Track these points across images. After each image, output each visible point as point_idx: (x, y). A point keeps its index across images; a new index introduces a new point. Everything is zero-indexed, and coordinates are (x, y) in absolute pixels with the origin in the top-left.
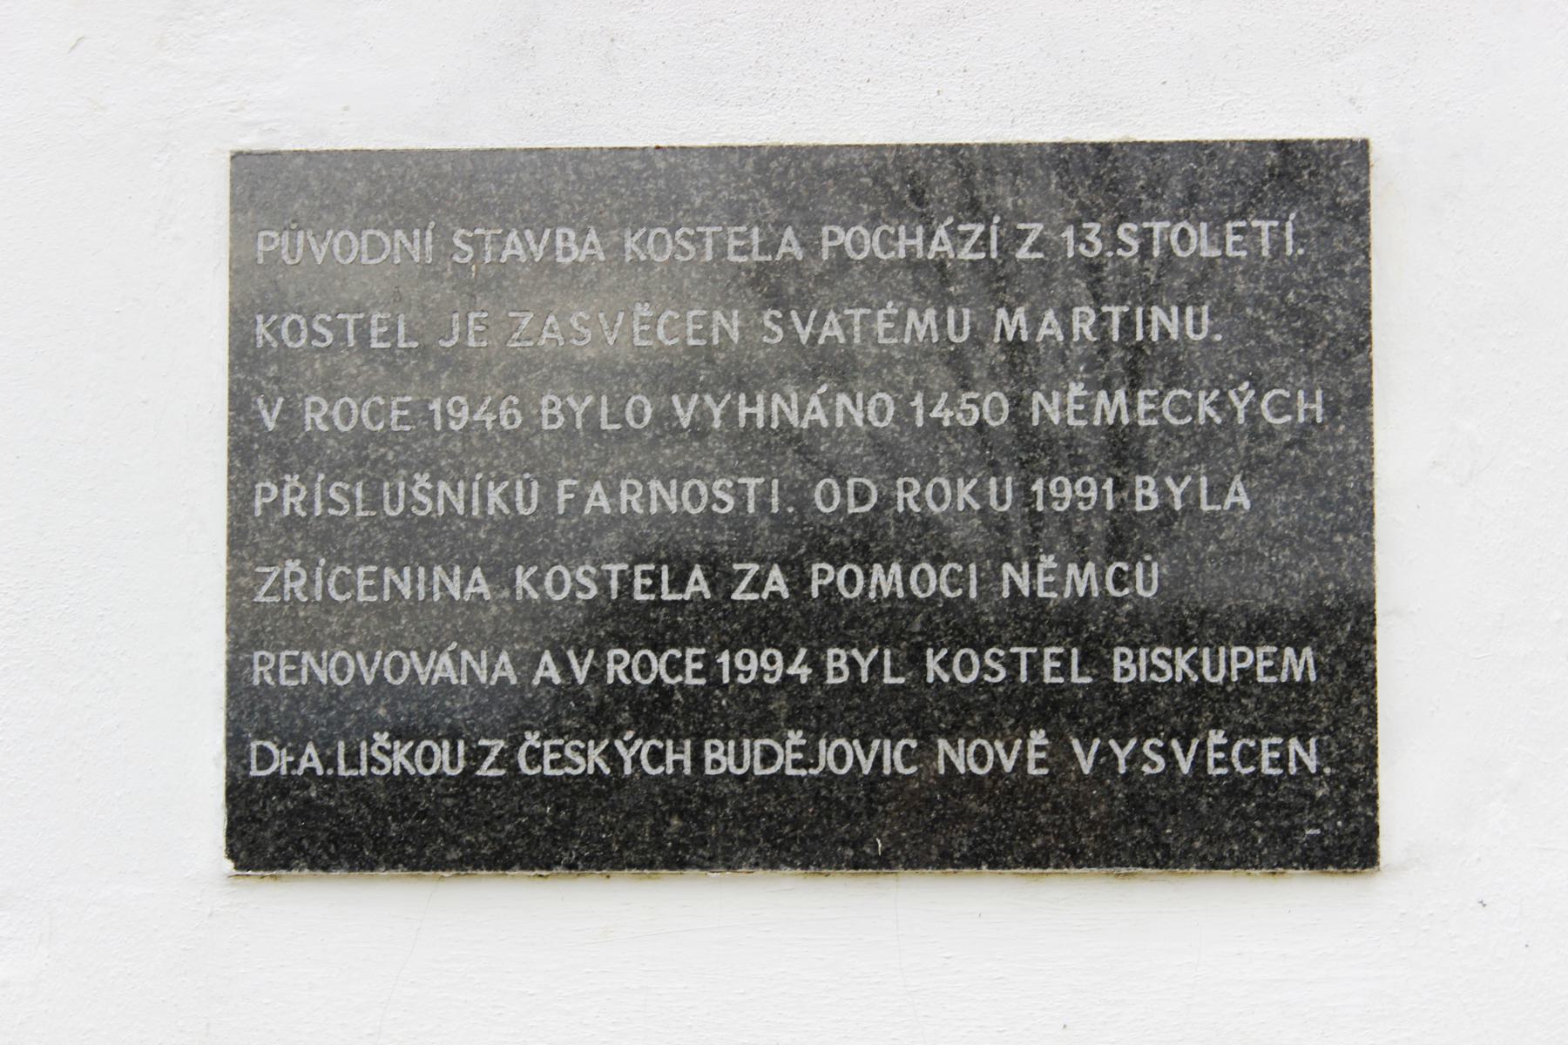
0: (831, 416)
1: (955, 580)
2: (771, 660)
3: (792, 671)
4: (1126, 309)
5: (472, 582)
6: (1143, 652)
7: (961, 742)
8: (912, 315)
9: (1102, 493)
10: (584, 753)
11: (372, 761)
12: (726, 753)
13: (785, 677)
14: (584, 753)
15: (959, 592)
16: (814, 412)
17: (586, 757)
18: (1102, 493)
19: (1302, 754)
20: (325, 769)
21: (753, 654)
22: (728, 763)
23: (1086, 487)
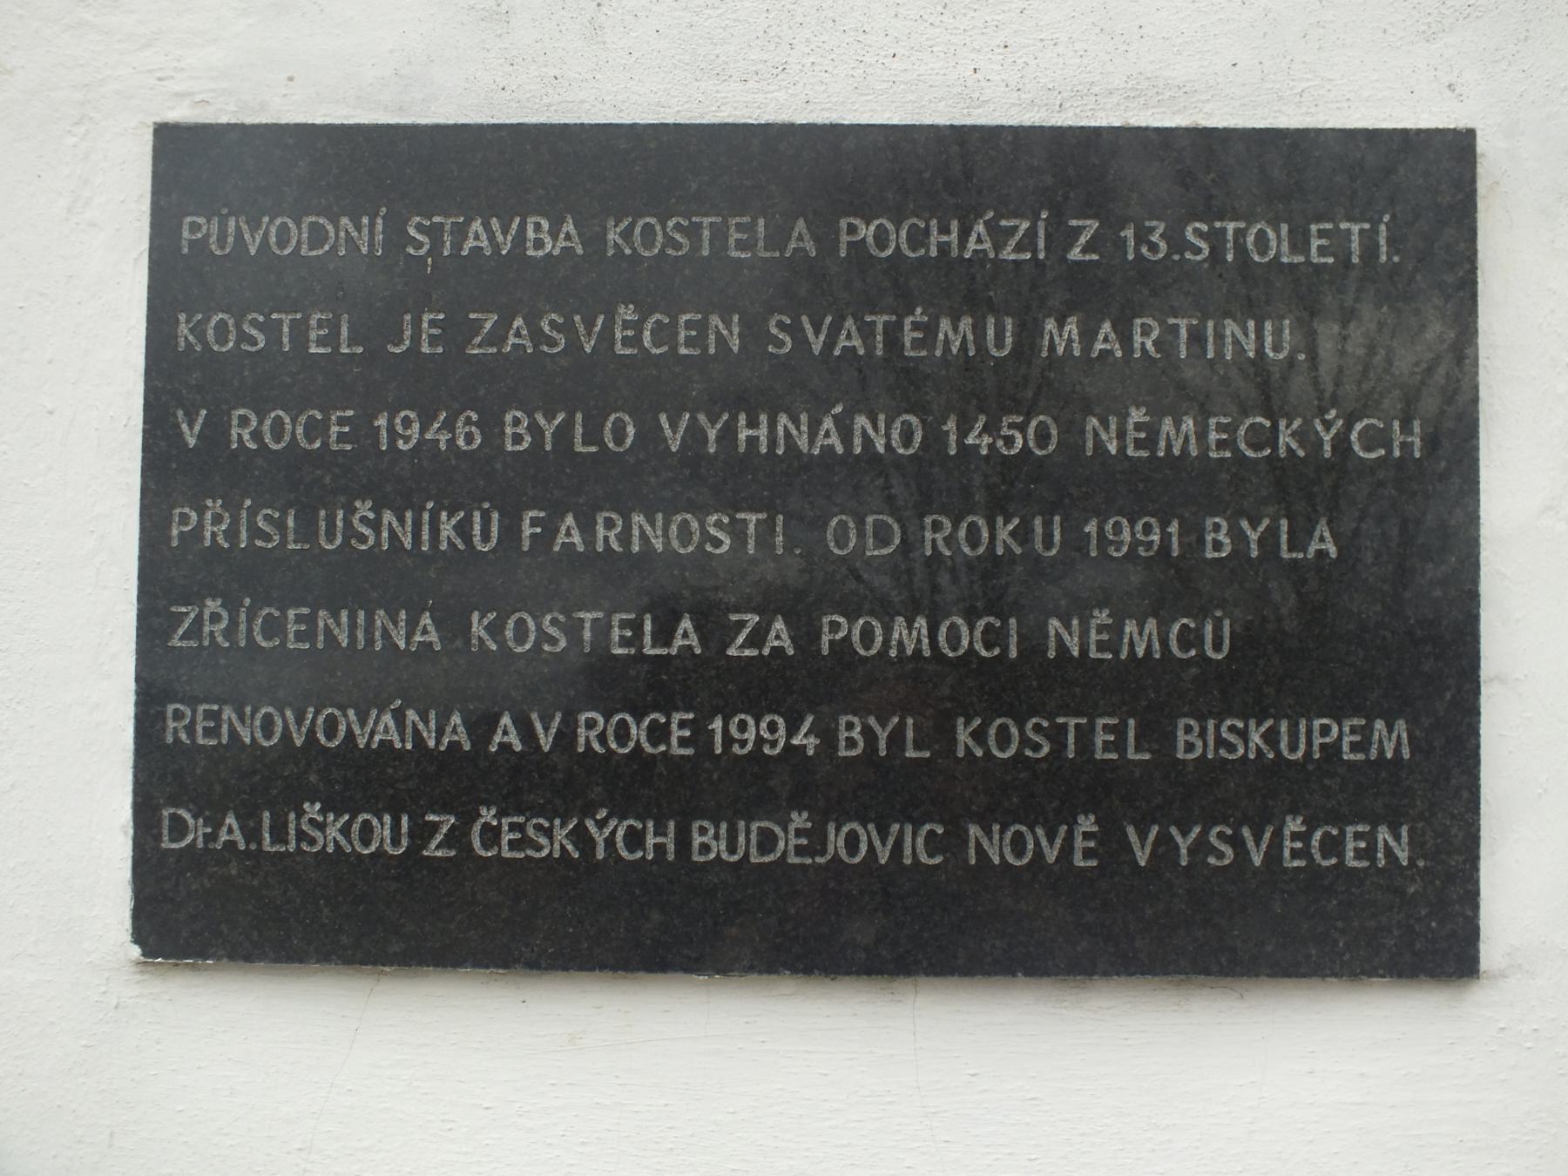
2: (772, 728)
11: (301, 835)
13: (789, 747)
14: (549, 833)
17: (324, 832)
21: (751, 721)
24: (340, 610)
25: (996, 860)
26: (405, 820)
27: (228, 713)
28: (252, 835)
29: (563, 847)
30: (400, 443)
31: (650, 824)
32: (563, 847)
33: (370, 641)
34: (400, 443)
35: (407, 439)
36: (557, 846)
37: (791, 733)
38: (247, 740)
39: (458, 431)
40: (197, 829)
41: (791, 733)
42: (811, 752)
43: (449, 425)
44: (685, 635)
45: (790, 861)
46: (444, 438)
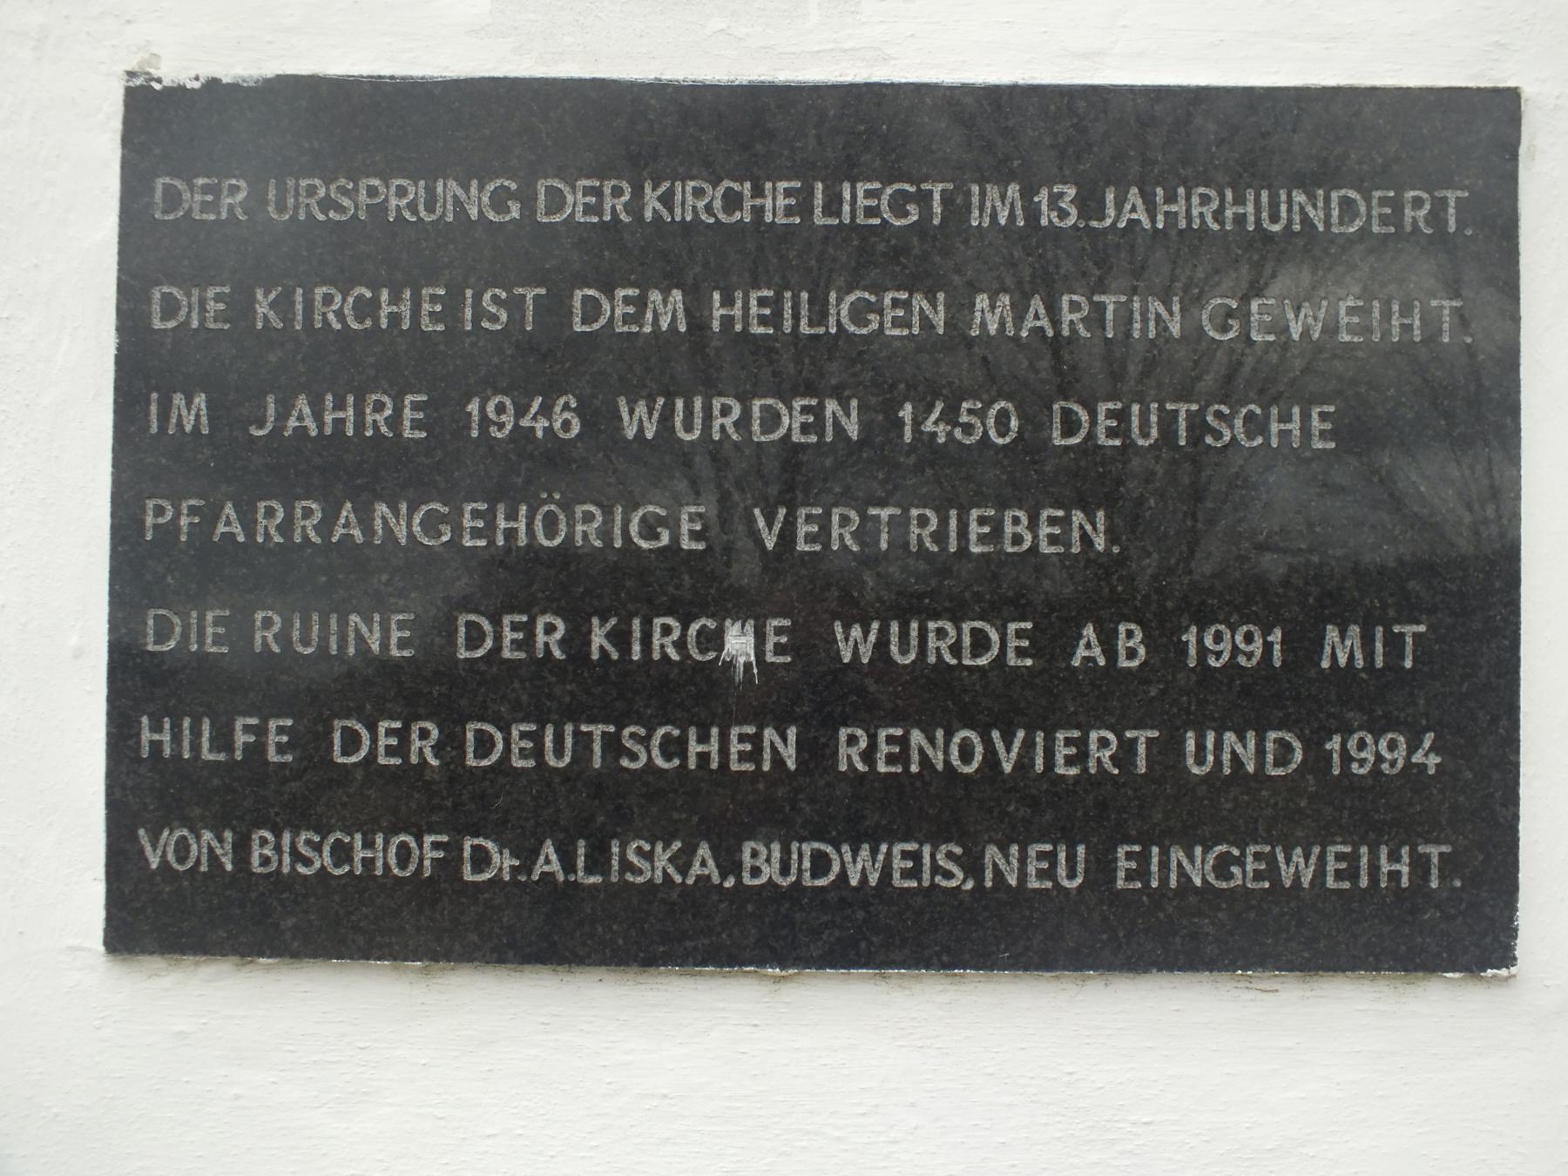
0: (368, 530)
1: (672, 749)
2: (1392, 746)
3: (1417, 758)
4: (1194, 407)
5: (1128, 207)
6: (287, 838)
7: (1198, 850)
8: (655, 296)
9: (1268, 647)
10: (649, 856)
11: (626, 866)
12: (768, 860)
13: (1409, 764)
14: (649, 856)
15: (676, 762)
16: (228, 523)
17: (652, 862)
18: (1268, 647)
19: (1001, 863)
20: (724, 877)
21: (1369, 739)
22: (770, 872)
23: (1249, 638)
24: (790, 618)
25: (1198, 882)
26: (1081, 850)
27: (917, 737)
28: (568, 864)
29: (664, 871)
30: (493, 429)
31: (358, 837)
32: (664, 871)
33: (342, 645)
34: (493, 429)
35: (501, 426)
36: (659, 873)
37: (1412, 750)
38: (940, 767)
39: (555, 417)
40: (503, 862)
41: (1412, 750)
42: (1432, 772)
43: (546, 411)
44: (1088, 646)
45: (1030, 886)
46: (942, 429)
